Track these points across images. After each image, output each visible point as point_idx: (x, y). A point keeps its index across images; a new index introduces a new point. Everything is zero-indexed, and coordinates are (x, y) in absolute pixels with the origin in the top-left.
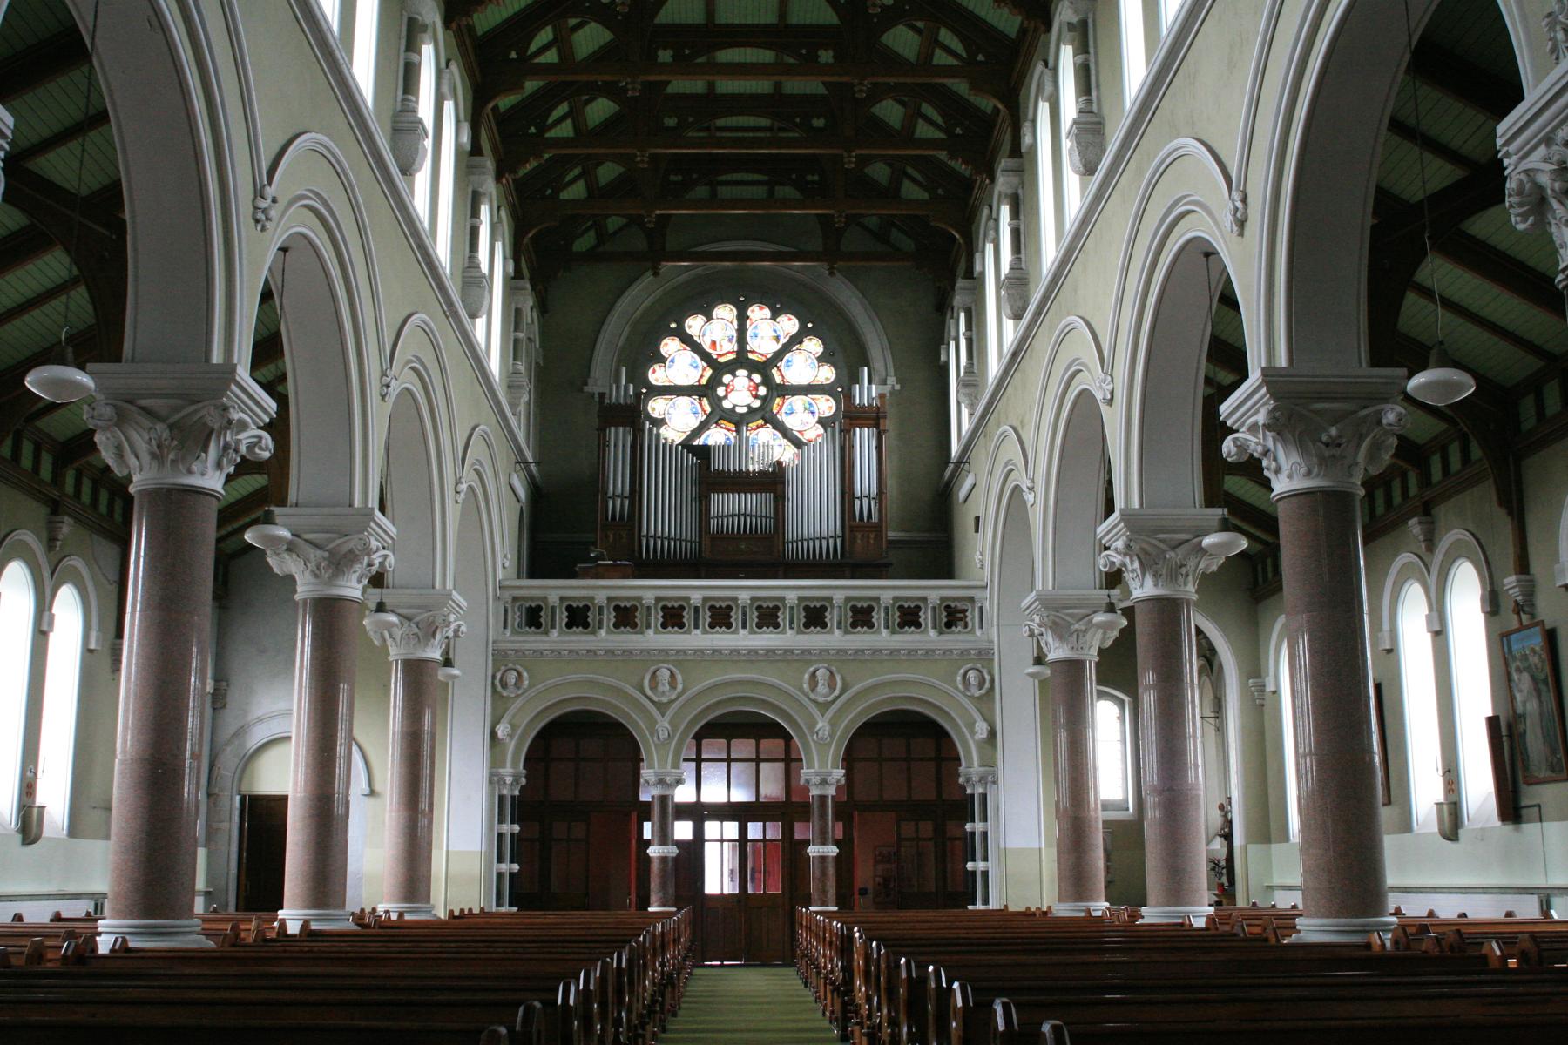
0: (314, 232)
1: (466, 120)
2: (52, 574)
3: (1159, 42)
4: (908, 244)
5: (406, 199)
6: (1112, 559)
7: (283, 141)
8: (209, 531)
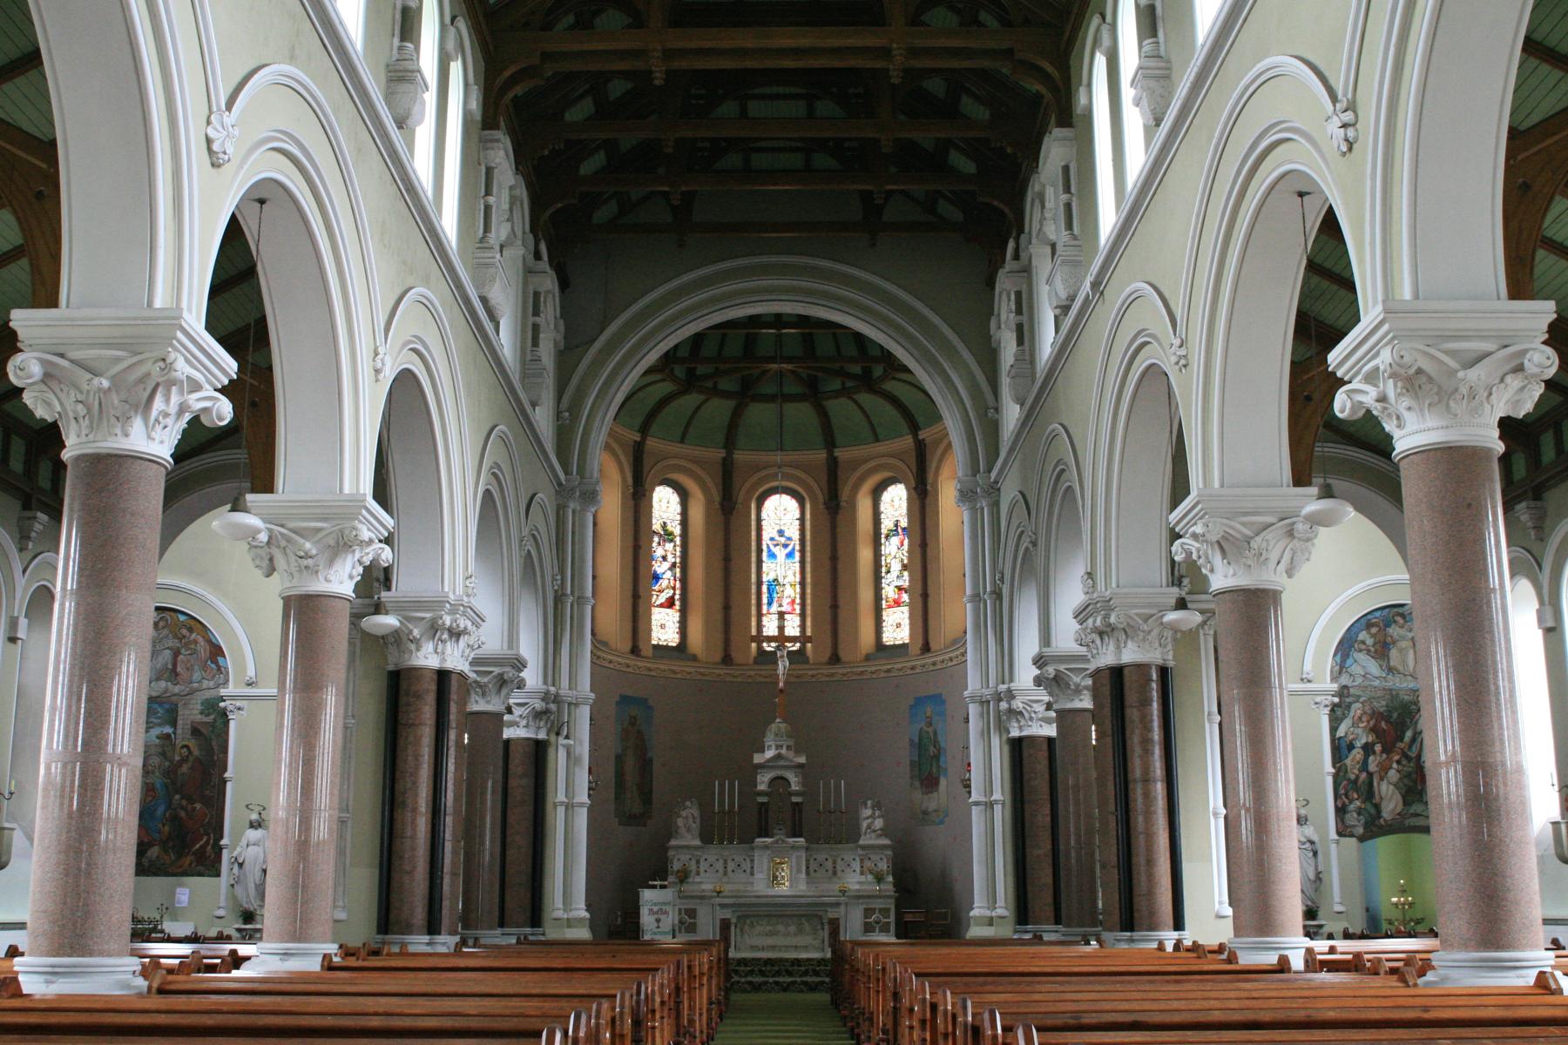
0: (287, 176)
1: (476, 84)
2: (24, 571)
3: (1194, 54)
4: (956, 215)
5: (435, 220)
6: (1186, 547)
7: (254, 66)
8: (343, 625)
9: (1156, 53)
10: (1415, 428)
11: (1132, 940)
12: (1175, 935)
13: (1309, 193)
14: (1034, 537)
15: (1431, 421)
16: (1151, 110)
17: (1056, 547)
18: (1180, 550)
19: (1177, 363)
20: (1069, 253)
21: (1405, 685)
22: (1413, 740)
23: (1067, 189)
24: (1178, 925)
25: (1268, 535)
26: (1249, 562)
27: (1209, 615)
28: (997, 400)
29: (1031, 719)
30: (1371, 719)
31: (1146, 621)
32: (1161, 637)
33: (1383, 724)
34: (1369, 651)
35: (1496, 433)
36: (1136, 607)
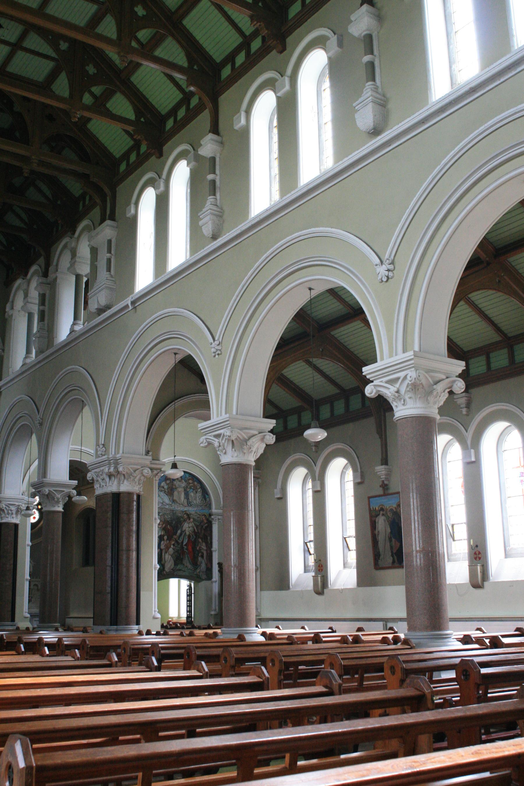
9: (215, 204)
10: (412, 406)
11: (117, 630)
12: (136, 627)
13: (313, 289)
14: (41, 420)
15: (419, 404)
16: (212, 230)
17: (56, 428)
18: (205, 441)
19: (214, 353)
20: (109, 283)
21: (179, 509)
22: (181, 534)
23: (109, 251)
24: (138, 623)
25: (253, 440)
26: (245, 451)
27: (159, 471)
28: (4, 345)
29: (8, 514)
30: (164, 524)
31: (135, 471)
32: (140, 480)
33: (169, 526)
34: (165, 491)
35: (437, 411)
36: (132, 464)
